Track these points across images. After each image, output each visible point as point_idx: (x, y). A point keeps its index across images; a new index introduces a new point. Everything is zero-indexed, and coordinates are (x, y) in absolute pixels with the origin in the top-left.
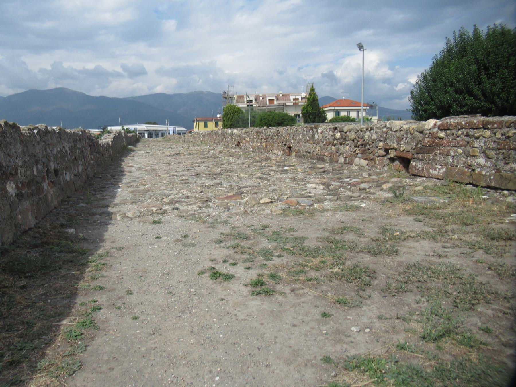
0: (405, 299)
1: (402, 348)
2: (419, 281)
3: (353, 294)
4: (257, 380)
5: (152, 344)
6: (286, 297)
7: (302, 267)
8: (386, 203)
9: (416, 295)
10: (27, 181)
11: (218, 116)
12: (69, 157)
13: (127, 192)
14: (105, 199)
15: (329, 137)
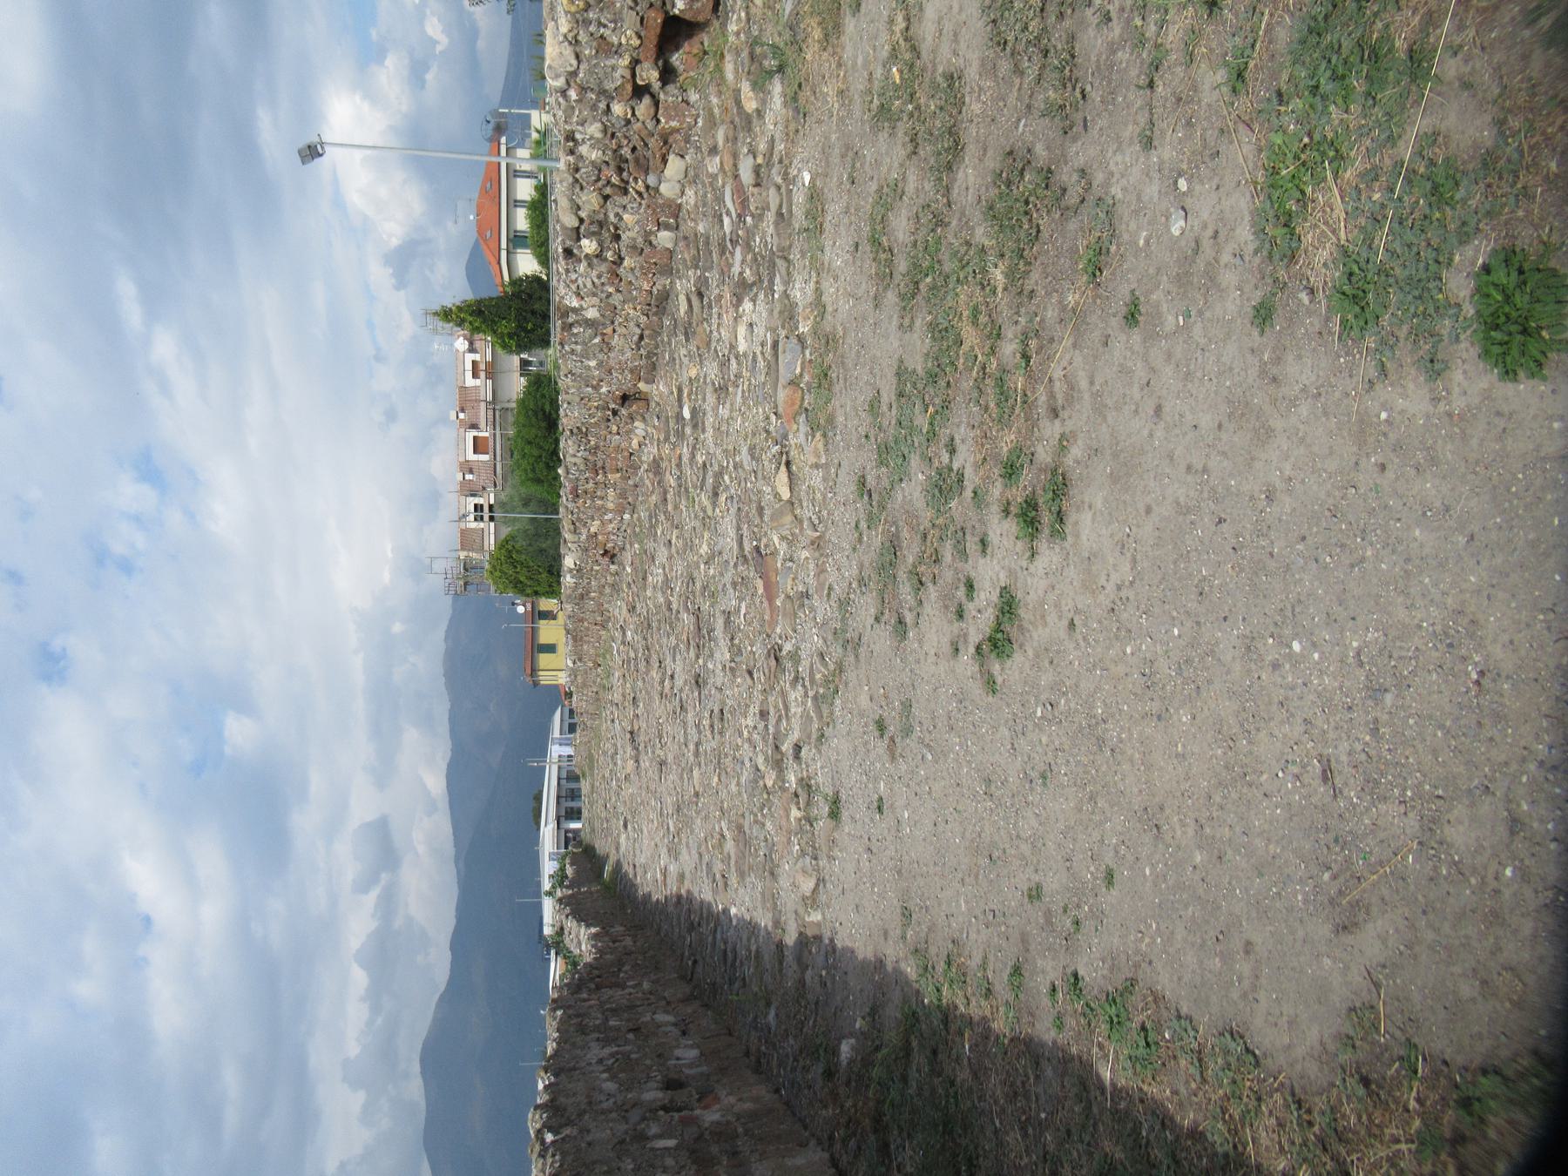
0: (1094, 59)
1: (1240, 75)
2: (1042, 10)
3: (1072, 225)
4: (1310, 528)
5: (1185, 833)
6: (1073, 434)
7: (988, 381)
8: (802, 101)
9: (1082, 23)
10: (694, 1167)
11: (521, 609)
12: (628, 1048)
13: (741, 891)
14: (757, 951)
15: (595, 273)
